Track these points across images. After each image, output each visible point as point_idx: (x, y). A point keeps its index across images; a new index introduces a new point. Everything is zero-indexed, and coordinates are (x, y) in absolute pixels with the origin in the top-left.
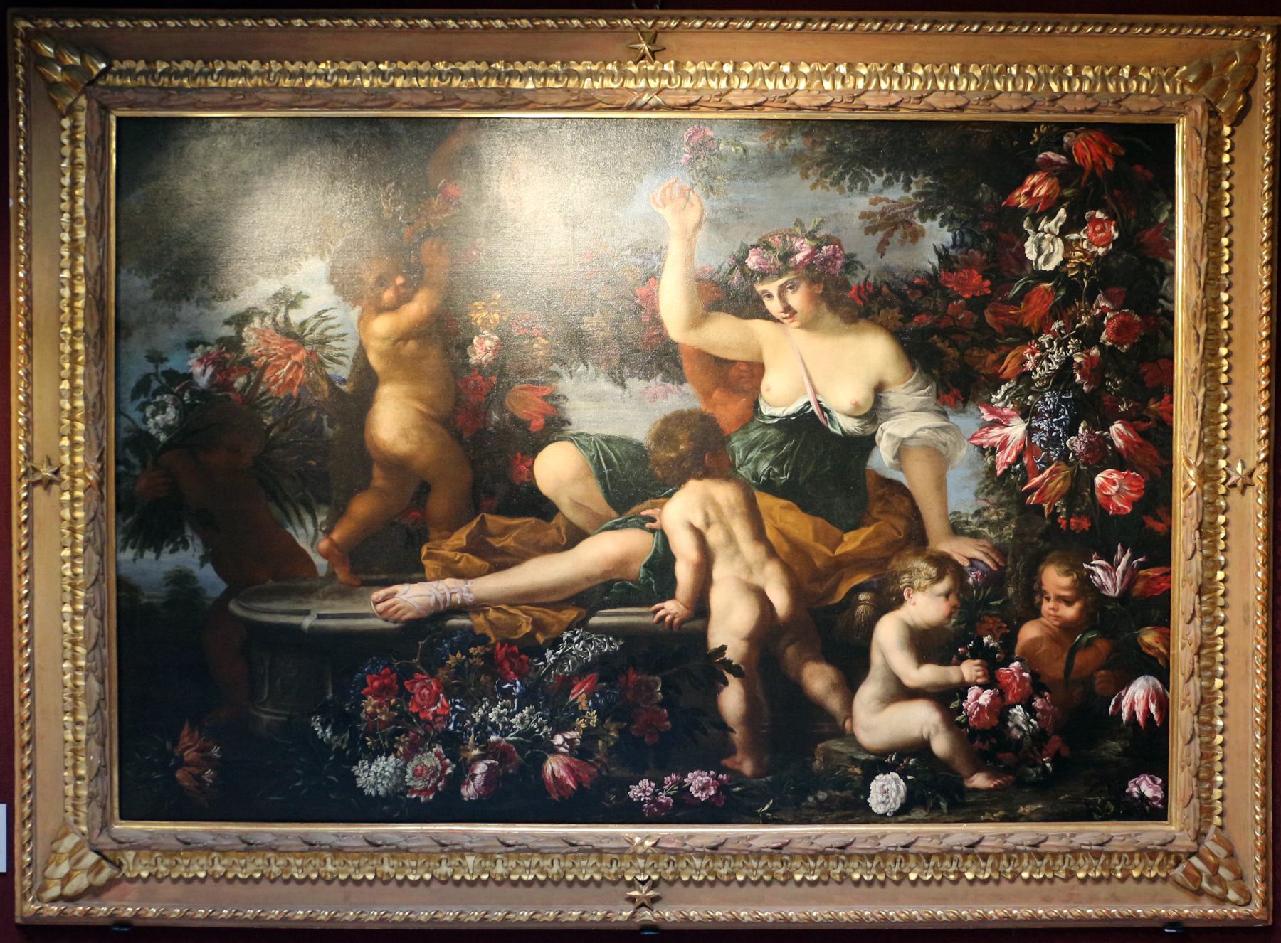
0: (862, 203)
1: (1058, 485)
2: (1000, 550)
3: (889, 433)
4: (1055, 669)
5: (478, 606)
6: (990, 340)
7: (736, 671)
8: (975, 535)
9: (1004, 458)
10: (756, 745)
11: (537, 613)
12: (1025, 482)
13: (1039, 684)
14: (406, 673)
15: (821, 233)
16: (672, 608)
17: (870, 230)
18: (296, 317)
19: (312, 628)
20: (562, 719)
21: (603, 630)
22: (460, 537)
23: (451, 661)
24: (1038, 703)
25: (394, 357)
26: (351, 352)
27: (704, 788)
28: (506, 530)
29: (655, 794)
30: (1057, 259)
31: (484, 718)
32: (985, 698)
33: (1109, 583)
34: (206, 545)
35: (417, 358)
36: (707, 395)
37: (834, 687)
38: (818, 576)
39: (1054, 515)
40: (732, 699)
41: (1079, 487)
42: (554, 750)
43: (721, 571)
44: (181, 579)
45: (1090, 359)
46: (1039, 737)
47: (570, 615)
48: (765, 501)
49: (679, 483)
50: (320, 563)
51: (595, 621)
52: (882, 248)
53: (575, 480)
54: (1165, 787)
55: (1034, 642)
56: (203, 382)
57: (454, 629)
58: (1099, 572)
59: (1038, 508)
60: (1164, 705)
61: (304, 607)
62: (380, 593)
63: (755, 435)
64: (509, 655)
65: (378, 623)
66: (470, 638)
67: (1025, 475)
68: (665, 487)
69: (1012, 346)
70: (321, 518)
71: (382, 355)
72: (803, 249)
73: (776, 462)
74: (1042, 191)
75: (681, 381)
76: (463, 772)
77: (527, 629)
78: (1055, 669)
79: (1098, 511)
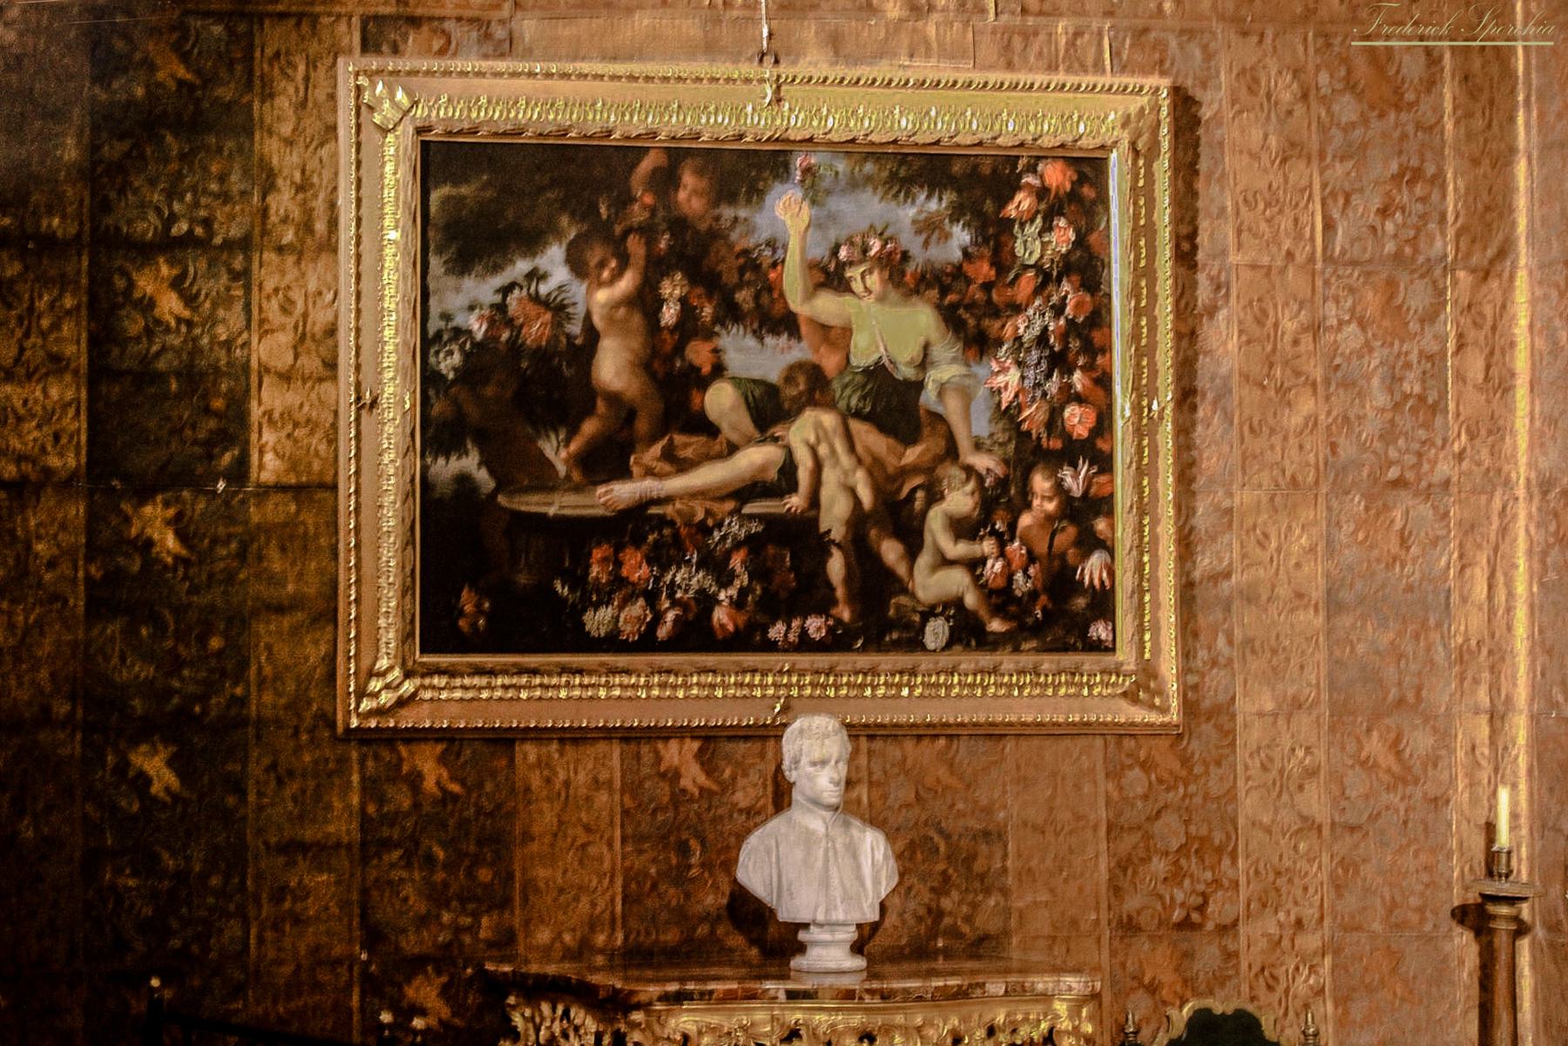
0: (911, 212)
1: (1042, 416)
2: (1006, 462)
3: (933, 377)
4: (1042, 548)
5: (668, 500)
6: (995, 312)
7: (839, 546)
8: (990, 451)
9: (1007, 397)
10: (851, 599)
11: (708, 504)
12: (1020, 412)
13: (1031, 558)
14: (619, 548)
15: (886, 235)
16: (796, 502)
17: (918, 232)
18: (544, 289)
19: (555, 516)
20: (725, 579)
21: (751, 517)
22: (657, 449)
23: (651, 538)
24: (1031, 571)
25: (610, 320)
26: (582, 315)
27: (819, 629)
28: (686, 445)
29: (786, 635)
30: (1036, 255)
31: (673, 581)
32: (999, 566)
33: (1075, 487)
34: (481, 453)
35: (626, 320)
36: (817, 351)
37: (902, 558)
38: (892, 479)
39: (1039, 439)
40: (836, 566)
41: (1054, 421)
42: (719, 602)
43: (830, 477)
44: (463, 480)
45: (1058, 327)
46: (1033, 595)
47: (730, 505)
48: (856, 426)
49: (799, 411)
50: (562, 469)
51: (747, 510)
52: (926, 244)
53: (732, 408)
54: (1114, 630)
55: (1029, 527)
56: (479, 336)
57: (652, 516)
58: (1067, 474)
59: (1028, 433)
60: (1112, 574)
61: (548, 500)
62: (601, 490)
63: (847, 379)
64: (691, 536)
65: (600, 512)
66: (663, 521)
67: (1020, 409)
68: (787, 415)
69: (1009, 317)
70: (562, 437)
71: (602, 318)
72: (875, 246)
73: (863, 398)
74: (1025, 205)
75: (800, 339)
76: (658, 618)
77: (700, 515)
78: (1042, 548)
79: (1066, 436)
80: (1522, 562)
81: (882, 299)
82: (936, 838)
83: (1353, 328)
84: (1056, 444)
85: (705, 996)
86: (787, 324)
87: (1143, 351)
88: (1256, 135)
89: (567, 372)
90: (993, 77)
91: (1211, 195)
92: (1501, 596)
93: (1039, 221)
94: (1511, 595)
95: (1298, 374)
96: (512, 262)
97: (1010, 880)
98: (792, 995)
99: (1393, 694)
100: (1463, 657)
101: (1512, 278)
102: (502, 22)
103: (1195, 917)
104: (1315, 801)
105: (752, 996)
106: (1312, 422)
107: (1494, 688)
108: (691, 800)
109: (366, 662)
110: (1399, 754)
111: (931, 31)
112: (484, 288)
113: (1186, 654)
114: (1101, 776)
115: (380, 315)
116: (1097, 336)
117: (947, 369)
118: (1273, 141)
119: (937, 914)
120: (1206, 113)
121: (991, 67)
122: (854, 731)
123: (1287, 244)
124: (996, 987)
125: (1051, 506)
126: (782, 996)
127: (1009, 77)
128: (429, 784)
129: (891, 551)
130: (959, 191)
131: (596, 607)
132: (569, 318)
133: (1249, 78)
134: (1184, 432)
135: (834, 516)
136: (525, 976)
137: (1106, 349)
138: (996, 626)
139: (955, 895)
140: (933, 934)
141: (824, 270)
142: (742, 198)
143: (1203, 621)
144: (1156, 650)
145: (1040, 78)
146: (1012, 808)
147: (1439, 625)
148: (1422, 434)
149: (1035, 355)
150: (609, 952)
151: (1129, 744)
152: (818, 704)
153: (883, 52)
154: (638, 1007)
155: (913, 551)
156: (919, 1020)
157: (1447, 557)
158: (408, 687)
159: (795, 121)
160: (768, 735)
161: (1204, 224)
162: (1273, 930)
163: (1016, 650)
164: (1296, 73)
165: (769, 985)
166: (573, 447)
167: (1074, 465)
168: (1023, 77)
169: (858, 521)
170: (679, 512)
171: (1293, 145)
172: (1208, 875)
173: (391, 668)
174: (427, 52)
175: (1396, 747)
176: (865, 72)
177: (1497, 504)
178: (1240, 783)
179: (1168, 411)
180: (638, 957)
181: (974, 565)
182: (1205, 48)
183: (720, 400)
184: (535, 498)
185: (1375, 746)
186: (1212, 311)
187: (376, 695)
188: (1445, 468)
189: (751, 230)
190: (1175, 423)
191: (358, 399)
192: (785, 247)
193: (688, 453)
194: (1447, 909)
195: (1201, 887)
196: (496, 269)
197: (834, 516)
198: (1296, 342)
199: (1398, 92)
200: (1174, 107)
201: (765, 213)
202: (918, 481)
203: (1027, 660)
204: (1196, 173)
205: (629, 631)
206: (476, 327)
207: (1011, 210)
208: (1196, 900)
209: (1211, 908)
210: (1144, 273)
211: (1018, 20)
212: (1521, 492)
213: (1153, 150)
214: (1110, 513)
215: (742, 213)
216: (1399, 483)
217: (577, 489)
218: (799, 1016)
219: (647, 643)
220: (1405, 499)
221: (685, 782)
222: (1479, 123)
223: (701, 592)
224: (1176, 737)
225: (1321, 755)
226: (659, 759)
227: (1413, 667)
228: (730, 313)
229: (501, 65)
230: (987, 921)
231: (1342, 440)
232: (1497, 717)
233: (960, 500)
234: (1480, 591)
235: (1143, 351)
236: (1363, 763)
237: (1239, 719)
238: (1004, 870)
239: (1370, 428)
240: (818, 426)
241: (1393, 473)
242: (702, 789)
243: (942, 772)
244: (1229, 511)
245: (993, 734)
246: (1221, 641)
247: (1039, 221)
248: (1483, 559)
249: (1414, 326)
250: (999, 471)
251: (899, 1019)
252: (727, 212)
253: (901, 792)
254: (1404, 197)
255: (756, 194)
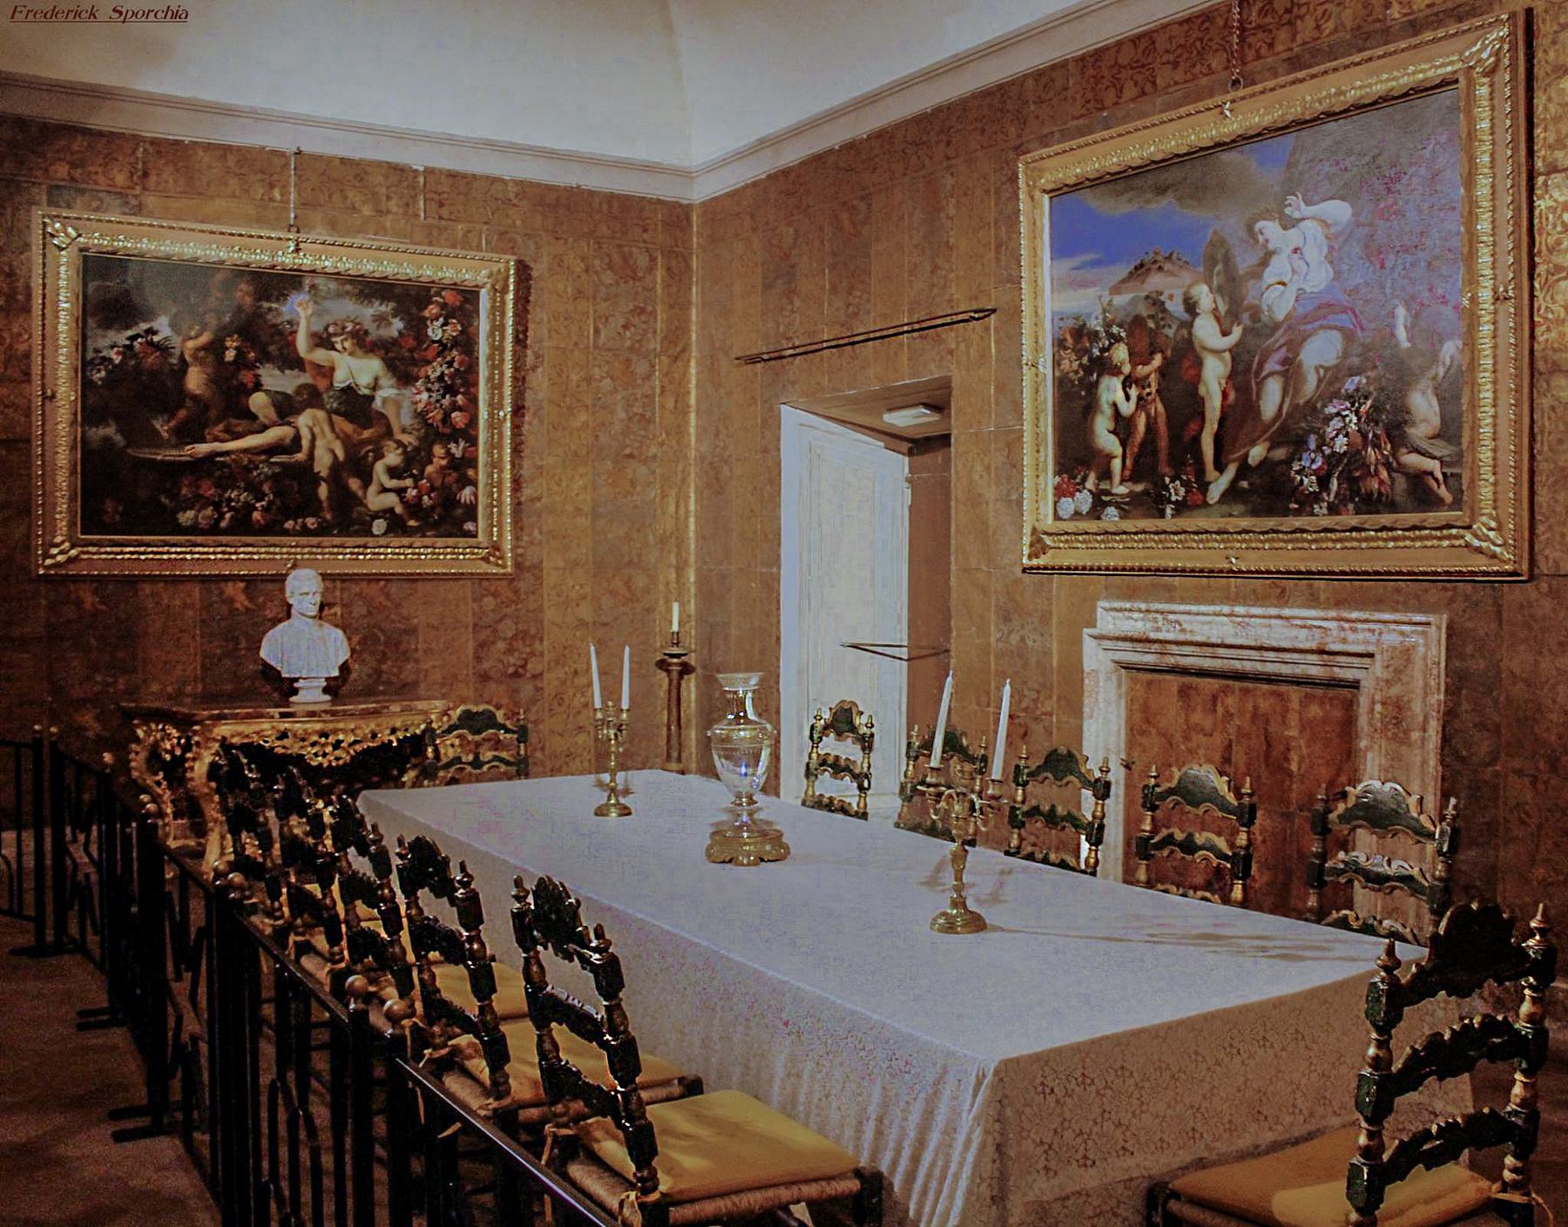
1: (439, 417)
2: (419, 439)
3: (380, 395)
4: (438, 483)
6: (414, 362)
7: (325, 481)
9: (420, 407)
10: (331, 509)
13: (432, 489)
14: (199, 478)
16: (300, 456)
18: (156, 339)
20: (260, 496)
22: (221, 427)
25: (195, 357)
28: (238, 425)
40: (323, 491)
41: (446, 418)
43: (319, 443)
46: (433, 507)
48: (335, 417)
50: (166, 435)
52: (378, 327)
56: (117, 362)
58: (452, 446)
72: (350, 327)
78: (438, 483)
79: (453, 426)
80: (692, 495)
81: (351, 354)
82: (380, 634)
83: (608, 380)
84: (447, 431)
85: (235, 716)
86: (297, 363)
87: (496, 387)
88: (560, 286)
89: (170, 384)
90: (420, 248)
91: (537, 314)
92: (682, 511)
93: (441, 319)
94: (687, 511)
95: (579, 401)
96: (137, 324)
97: (420, 654)
98: (283, 715)
99: (627, 559)
100: (663, 541)
101: (689, 361)
102: (136, 196)
103: (520, 670)
104: (585, 611)
105: (261, 716)
106: (586, 425)
107: (678, 554)
108: (240, 614)
109: (48, 538)
110: (629, 587)
111: (388, 224)
112: (122, 338)
113: (517, 538)
114: (470, 601)
115: (57, 348)
116: (470, 377)
117: (388, 391)
118: (569, 289)
119: (379, 673)
120: (534, 274)
121: (419, 244)
122: (325, 577)
123: (575, 338)
124: (395, 708)
125: (444, 462)
126: (277, 716)
127: (429, 249)
128: (87, 606)
129: (354, 484)
130: (398, 302)
131: (185, 510)
132: (171, 355)
133: (559, 260)
134: (516, 428)
135: (322, 464)
136: (142, 708)
137: (476, 384)
138: (412, 523)
139: (390, 663)
140: (377, 682)
141: (320, 337)
142: (274, 298)
143: (526, 522)
144: (500, 535)
145: (446, 251)
146: (420, 618)
147: (650, 525)
148: (643, 433)
149: (437, 386)
150: (194, 695)
151: (485, 584)
152: (310, 564)
153: (360, 231)
154: (197, 723)
155: (366, 484)
156: (352, 726)
157: (654, 492)
158: (73, 552)
159: (307, 262)
160: (280, 579)
161: (531, 326)
162: (562, 676)
163: (424, 536)
164: (583, 260)
165: (271, 710)
166: (172, 424)
167: (457, 442)
168: (437, 250)
169: (336, 467)
170: (233, 460)
171: (580, 292)
172: (528, 650)
173: (63, 542)
174: (88, 208)
175: (628, 584)
176: (349, 241)
177: (680, 468)
178: (545, 602)
179: (509, 417)
180: (209, 699)
181: (400, 492)
182: (536, 244)
183: (258, 401)
184: (147, 450)
185: (617, 584)
186: (534, 369)
187: (54, 556)
188: (653, 450)
189: (279, 314)
190: (512, 422)
191: (44, 393)
192: (298, 324)
193: (240, 429)
194: (654, 661)
195: (524, 656)
196: (128, 327)
197: (322, 464)
198: (578, 386)
199: (634, 272)
200: (517, 273)
201: (288, 305)
202: (370, 447)
203: (427, 541)
204: (528, 301)
205: (203, 522)
206: (114, 357)
207: (426, 313)
208: (520, 663)
209: (529, 666)
210: (497, 349)
211: (436, 222)
212: (692, 462)
213: (505, 290)
214: (475, 467)
215: (274, 305)
216: (630, 456)
217: (175, 447)
218: (287, 725)
219: (214, 530)
220: (633, 464)
221: (238, 605)
222: (675, 289)
223: (246, 502)
224: (511, 579)
225: (588, 590)
226: (222, 593)
227: (638, 545)
228: (265, 357)
229: (133, 219)
230: (408, 674)
231: (601, 434)
232: (680, 569)
233: (393, 458)
234: (672, 508)
235: (496, 387)
236: (611, 592)
237: (545, 571)
238: (416, 650)
239: (617, 428)
240: (314, 418)
241: (627, 451)
242: (247, 608)
243: (382, 599)
244: (541, 467)
245: (412, 579)
246: (536, 532)
247: (441, 319)
248: (673, 493)
249: (639, 382)
250: (416, 443)
251: (341, 725)
252: (266, 305)
253: (359, 610)
254: (636, 320)
255: (282, 297)
